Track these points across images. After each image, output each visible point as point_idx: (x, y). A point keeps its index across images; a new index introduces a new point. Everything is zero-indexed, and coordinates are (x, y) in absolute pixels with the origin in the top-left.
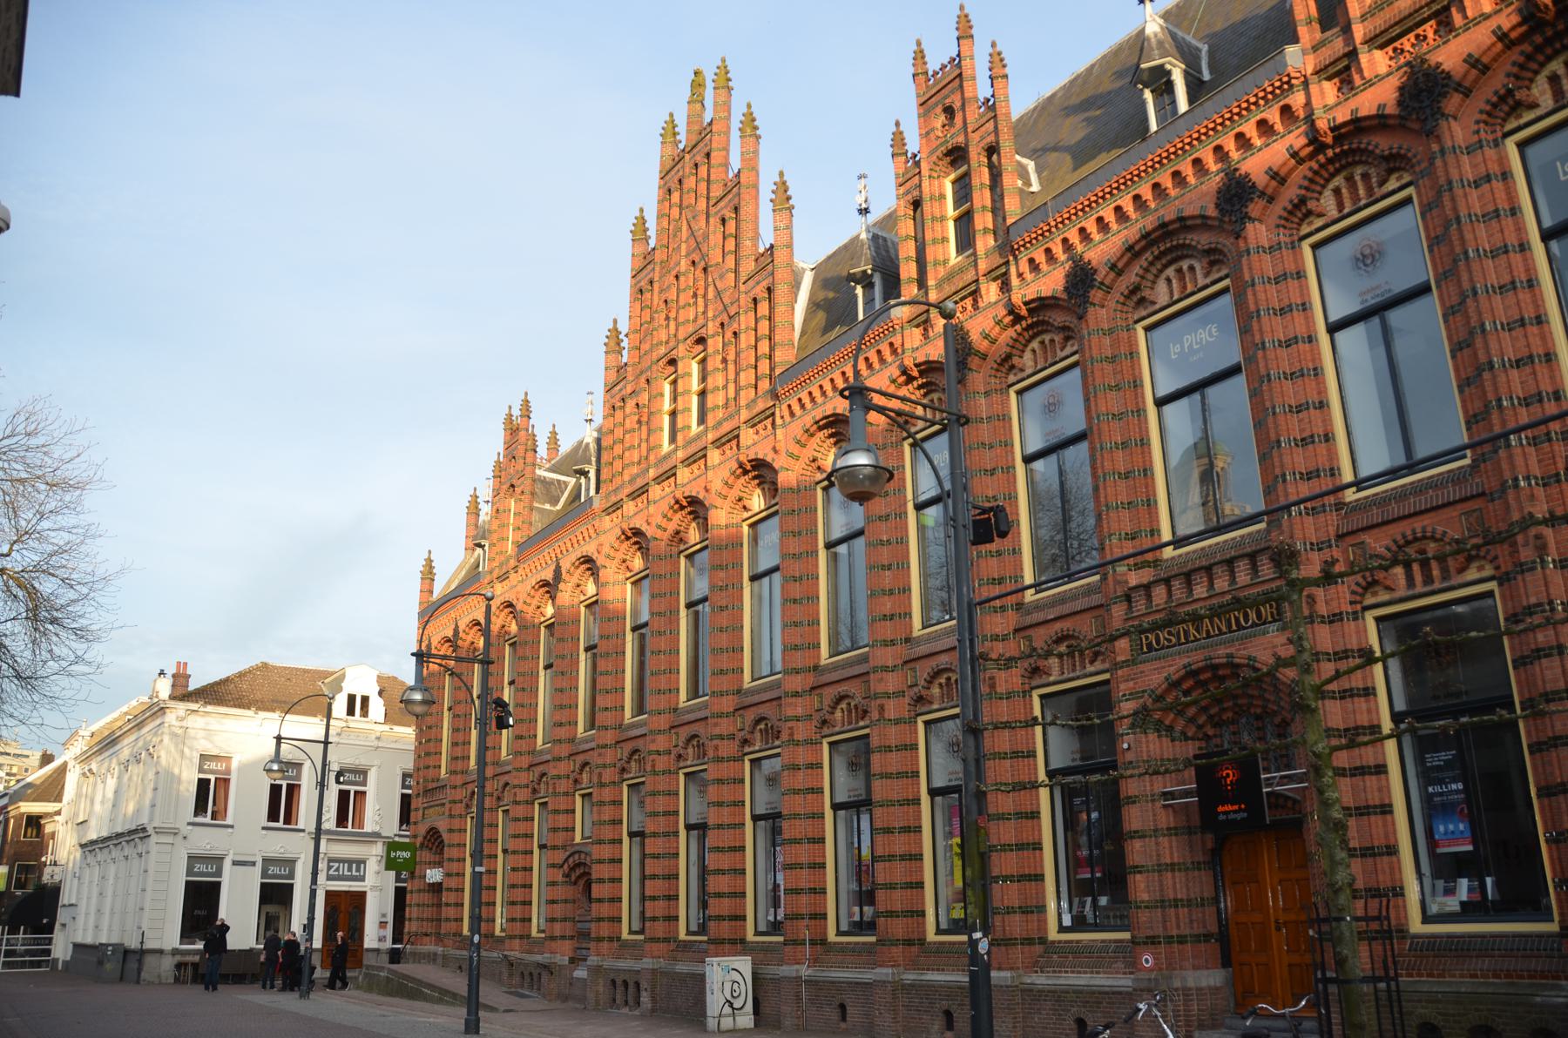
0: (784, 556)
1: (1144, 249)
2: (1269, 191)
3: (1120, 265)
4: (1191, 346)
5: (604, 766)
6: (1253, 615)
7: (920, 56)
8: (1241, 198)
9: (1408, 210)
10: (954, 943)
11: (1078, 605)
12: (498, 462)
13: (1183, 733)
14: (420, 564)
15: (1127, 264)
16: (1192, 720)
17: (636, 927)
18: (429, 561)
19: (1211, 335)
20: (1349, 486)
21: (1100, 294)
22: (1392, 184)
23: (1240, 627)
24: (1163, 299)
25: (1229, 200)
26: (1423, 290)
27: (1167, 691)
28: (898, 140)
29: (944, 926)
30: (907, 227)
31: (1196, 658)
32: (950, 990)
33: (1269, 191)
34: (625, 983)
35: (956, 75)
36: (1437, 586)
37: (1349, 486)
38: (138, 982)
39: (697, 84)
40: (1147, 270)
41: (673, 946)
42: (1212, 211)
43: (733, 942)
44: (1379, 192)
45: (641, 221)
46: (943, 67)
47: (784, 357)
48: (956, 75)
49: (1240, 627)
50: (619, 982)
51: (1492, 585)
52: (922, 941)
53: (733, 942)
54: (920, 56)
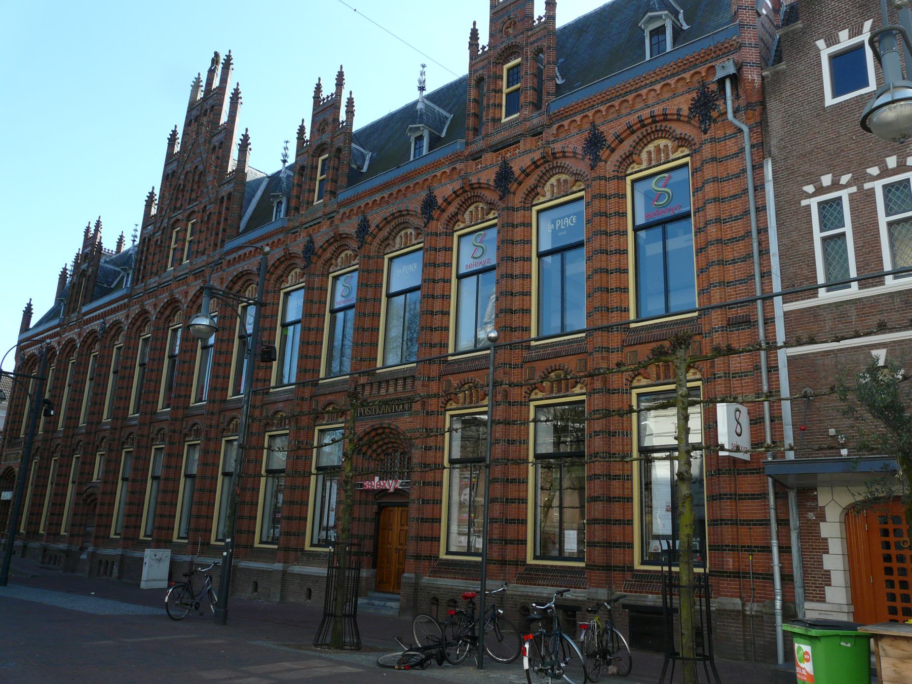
0: (424, 281)
1: (392, 220)
2: (443, 207)
3: (381, 226)
4: (560, 227)
5: (429, 396)
6: (401, 407)
7: (318, 88)
8: (506, 179)
9: (684, 170)
10: (574, 567)
11: (339, 388)
12: (78, 254)
13: (370, 456)
14: (23, 307)
15: (533, 171)
16: (375, 451)
17: (149, 533)
18: (30, 305)
19: (572, 222)
20: (888, 274)
21: (370, 238)
22: (678, 154)
23: (396, 411)
24: (397, 247)
25: (500, 180)
26: (579, 245)
27: (364, 436)
28: (474, 34)
29: (315, 542)
30: (473, 94)
31: (375, 423)
32: (316, 579)
33: (443, 207)
34: (107, 563)
35: (334, 102)
36: (662, 381)
37: (888, 274)
38: (223, 618)
39: (215, 60)
40: (392, 231)
41: (521, 569)
42: (492, 183)
43: (166, 542)
44: (672, 157)
45: (174, 133)
46: (328, 97)
47: (241, 230)
48: (334, 102)
49: (396, 411)
50: (104, 561)
51: (699, 383)
52: (302, 550)
53: (166, 542)
54: (318, 88)
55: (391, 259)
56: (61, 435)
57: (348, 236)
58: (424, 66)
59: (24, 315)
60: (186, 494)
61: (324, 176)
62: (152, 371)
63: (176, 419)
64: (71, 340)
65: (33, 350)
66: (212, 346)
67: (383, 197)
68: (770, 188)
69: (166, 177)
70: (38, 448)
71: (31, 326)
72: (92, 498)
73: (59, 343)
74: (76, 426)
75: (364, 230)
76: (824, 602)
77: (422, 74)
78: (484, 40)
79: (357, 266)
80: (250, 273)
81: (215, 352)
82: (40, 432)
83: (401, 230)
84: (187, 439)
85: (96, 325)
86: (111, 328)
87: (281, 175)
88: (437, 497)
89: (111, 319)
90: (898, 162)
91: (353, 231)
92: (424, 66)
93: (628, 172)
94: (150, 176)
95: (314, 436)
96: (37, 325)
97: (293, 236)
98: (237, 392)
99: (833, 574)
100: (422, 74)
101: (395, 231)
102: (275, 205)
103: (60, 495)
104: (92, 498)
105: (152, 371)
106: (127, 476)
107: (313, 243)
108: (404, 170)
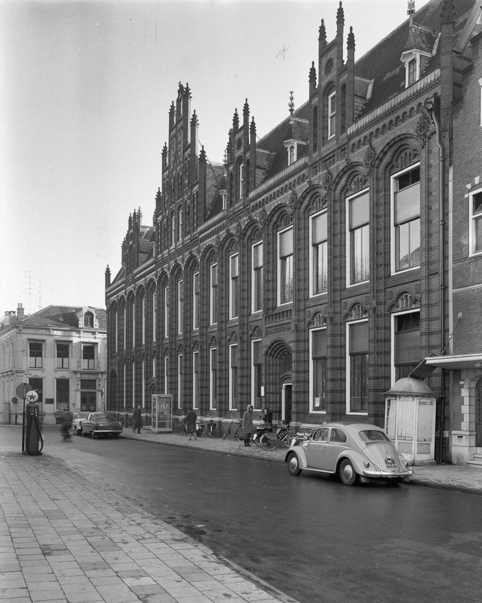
47: (111, 283)
55: (351, 201)
56: (168, 342)
57: (358, 164)
58: (292, 93)
59: (106, 276)
60: (441, 360)
61: (334, 113)
62: (243, 282)
63: (222, 330)
64: (131, 292)
65: (113, 298)
66: (262, 267)
67: (420, 104)
68: (451, 184)
69: (163, 185)
70: (144, 354)
71: (111, 283)
72: (153, 387)
73: (135, 289)
74: (177, 334)
75: (424, 127)
76: (461, 430)
77: (292, 98)
78: (147, 221)
79: (326, 209)
80: (285, 206)
81: (265, 271)
82: (154, 340)
83: (353, 178)
84: (347, 320)
85: (141, 282)
86: (272, 215)
87: (291, 122)
88: (343, 377)
89: (149, 277)
90: (474, 181)
91: (362, 160)
92: (292, 93)
93: (347, 196)
94: (154, 182)
95: (251, 346)
96: (114, 282)
97: (314, 170)
98: (284, 300)
99: (465, 415)
100: (292, 98)
101: (351, 178)
102: (289, 150)
103: (139, 386)
104: (153, 387)
105: (243, 282)
106: (322, 354)
107: (296, 194)
108: (402, 97)
